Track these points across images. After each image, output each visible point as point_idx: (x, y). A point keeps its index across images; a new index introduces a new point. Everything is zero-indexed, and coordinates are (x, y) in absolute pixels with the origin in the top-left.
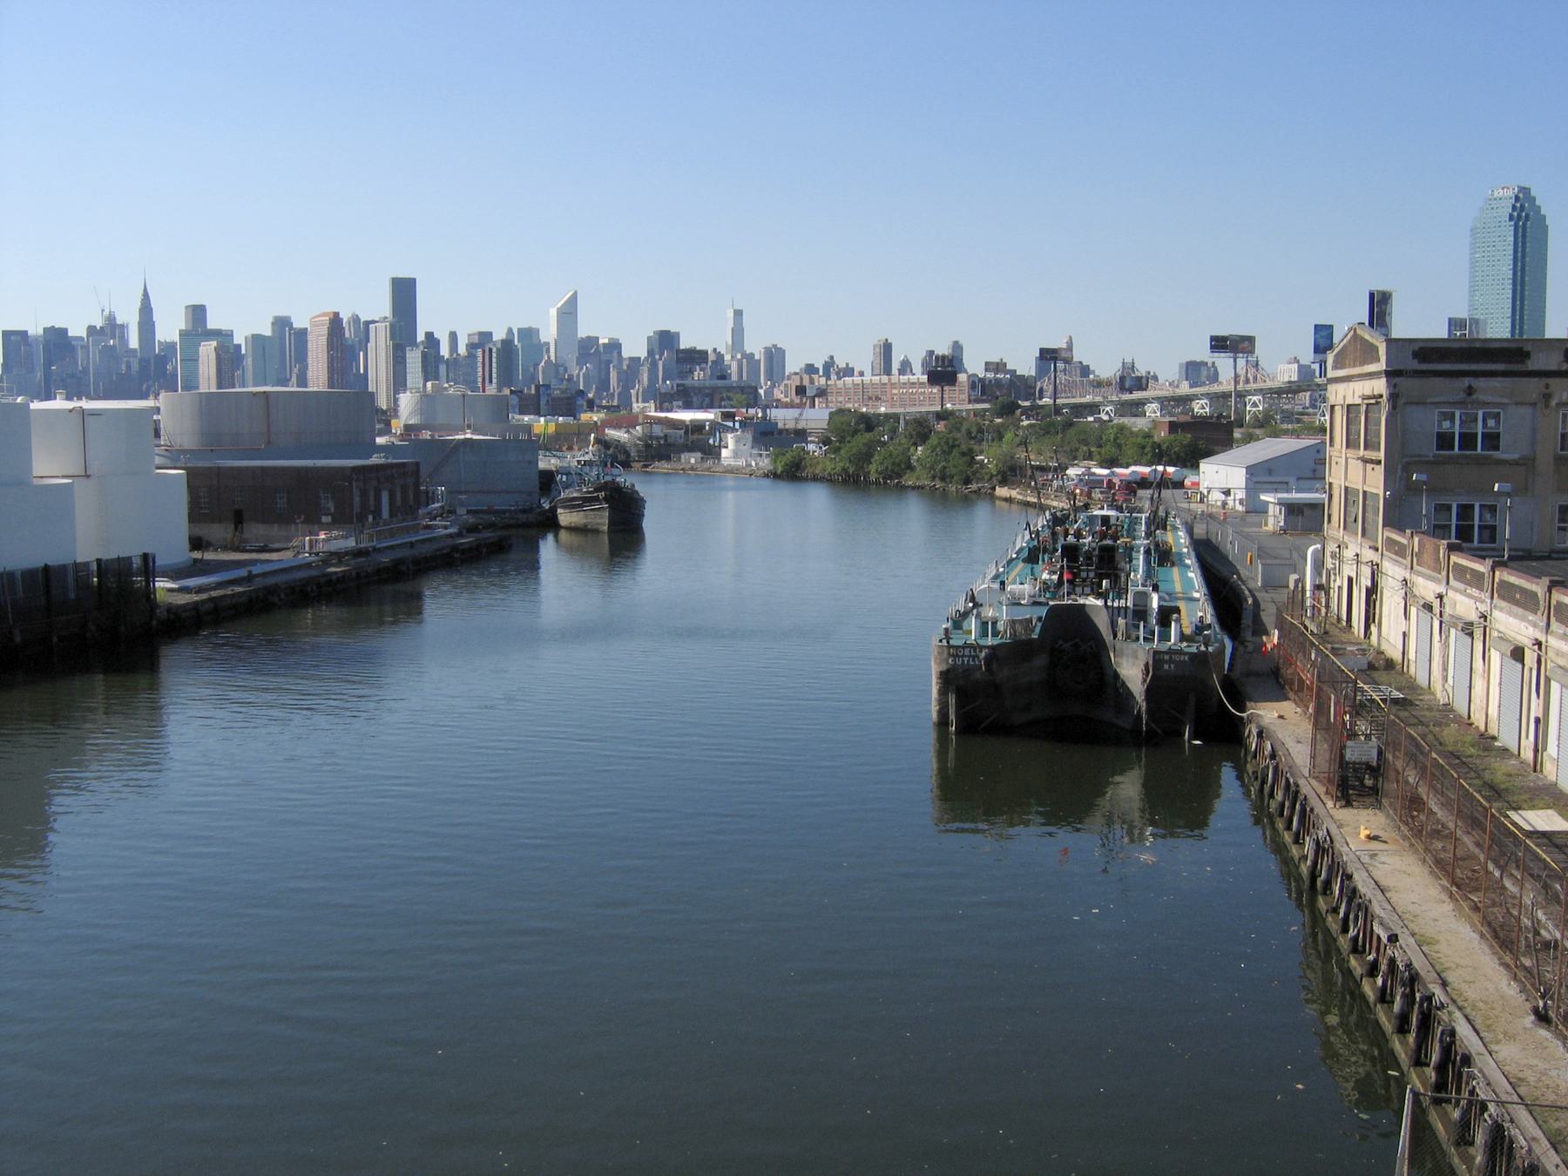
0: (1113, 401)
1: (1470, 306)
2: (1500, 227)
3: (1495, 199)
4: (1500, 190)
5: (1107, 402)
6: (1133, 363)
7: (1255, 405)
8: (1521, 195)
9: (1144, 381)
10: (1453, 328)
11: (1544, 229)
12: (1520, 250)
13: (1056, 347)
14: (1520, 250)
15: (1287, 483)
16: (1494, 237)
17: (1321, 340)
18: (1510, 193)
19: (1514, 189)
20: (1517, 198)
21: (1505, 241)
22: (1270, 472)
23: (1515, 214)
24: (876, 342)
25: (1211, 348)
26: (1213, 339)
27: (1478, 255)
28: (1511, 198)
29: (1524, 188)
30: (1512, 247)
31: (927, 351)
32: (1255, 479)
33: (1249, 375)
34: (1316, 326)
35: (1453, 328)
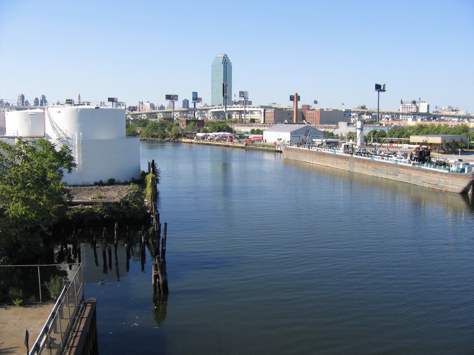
0: (131, 114)
1: (212, 87)
2: (220, 65)
3: (218, 57)
4: (219, 55)
5: (129, 114)
6: (142, 102)
7: (160, 116)
8: (225, 57)
9: (136, 108)
10: (240, 94)
11: (231, 66)
12: (225, 72)
13: (113, 98)
14: (225, 72)
15: (319, 136)
16: (218, 68)
17: (194, 96)
18: (222, 56)
19: (223, 55)
20: (224, 57)
21: (221, 69)
22: (296, 133)
23: (224, 62)
24: (19, 95)
25: (166, 98)
26: (166, 96)
27: (214, 73)
28: (222, 57)
29: (226, 55)
30: (223, 71)
31: (35, 98)
32: (292, 136)
33: (140, 106)
34: (193, 92)
35: (240, 94)
